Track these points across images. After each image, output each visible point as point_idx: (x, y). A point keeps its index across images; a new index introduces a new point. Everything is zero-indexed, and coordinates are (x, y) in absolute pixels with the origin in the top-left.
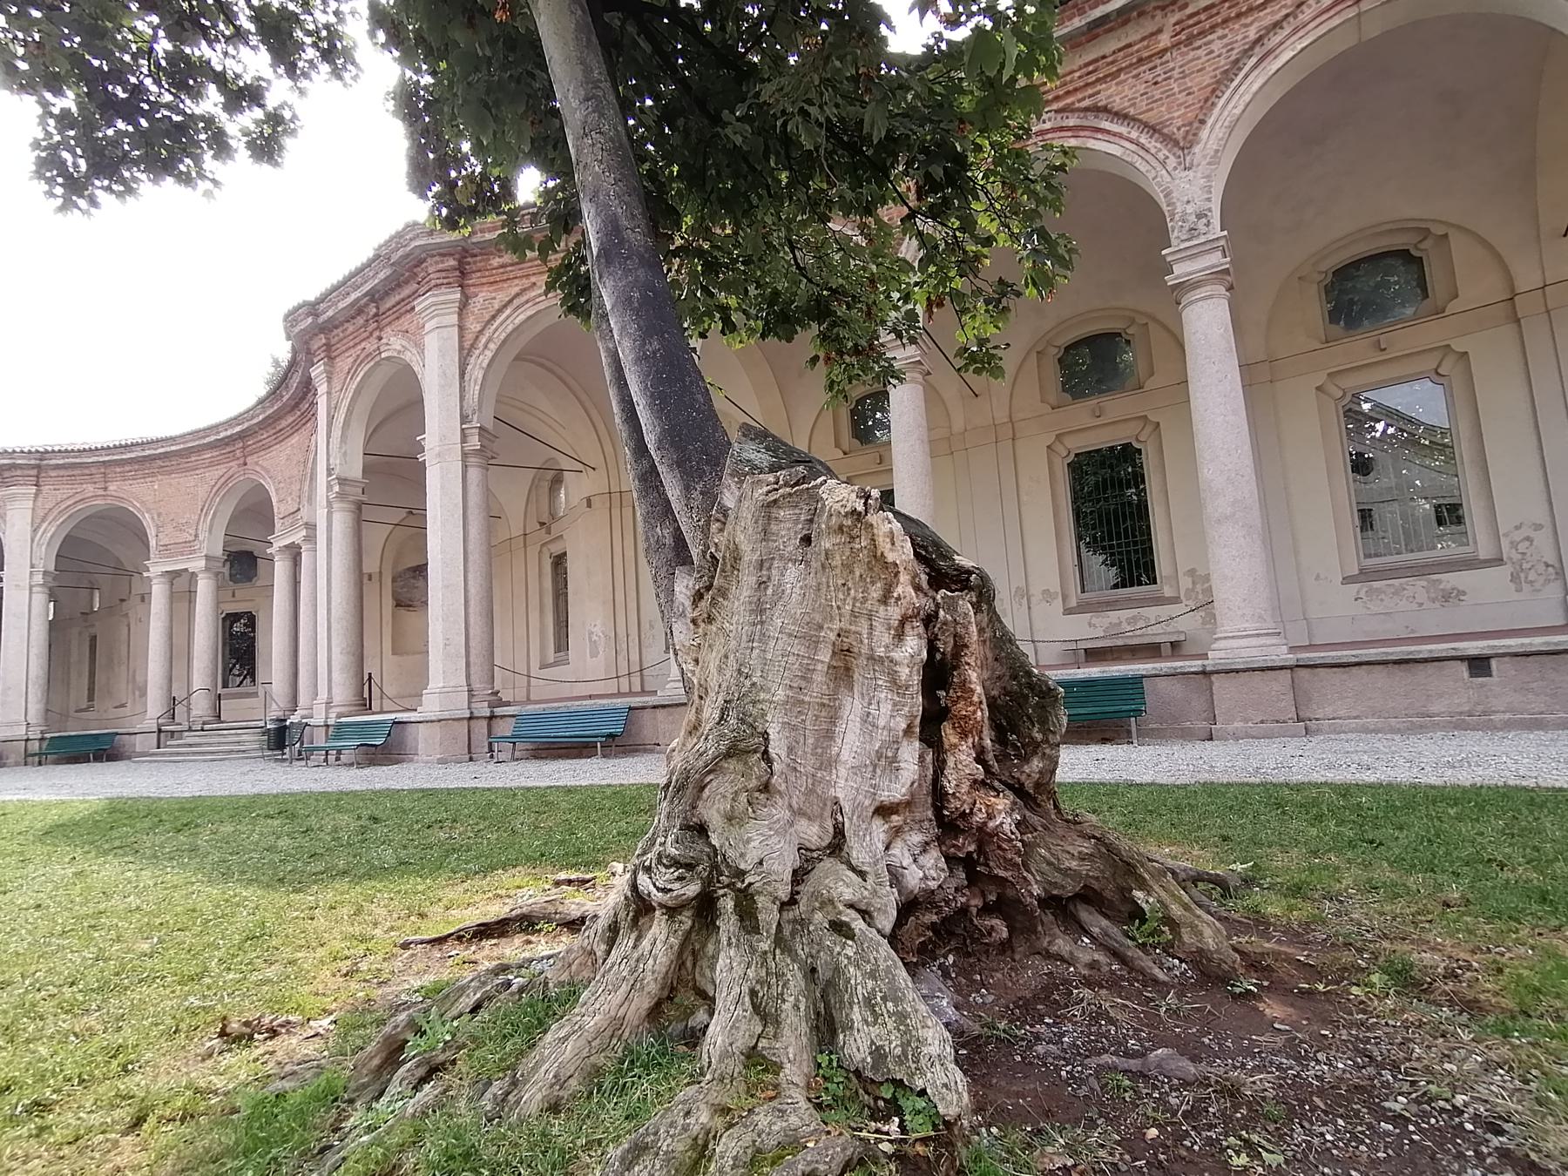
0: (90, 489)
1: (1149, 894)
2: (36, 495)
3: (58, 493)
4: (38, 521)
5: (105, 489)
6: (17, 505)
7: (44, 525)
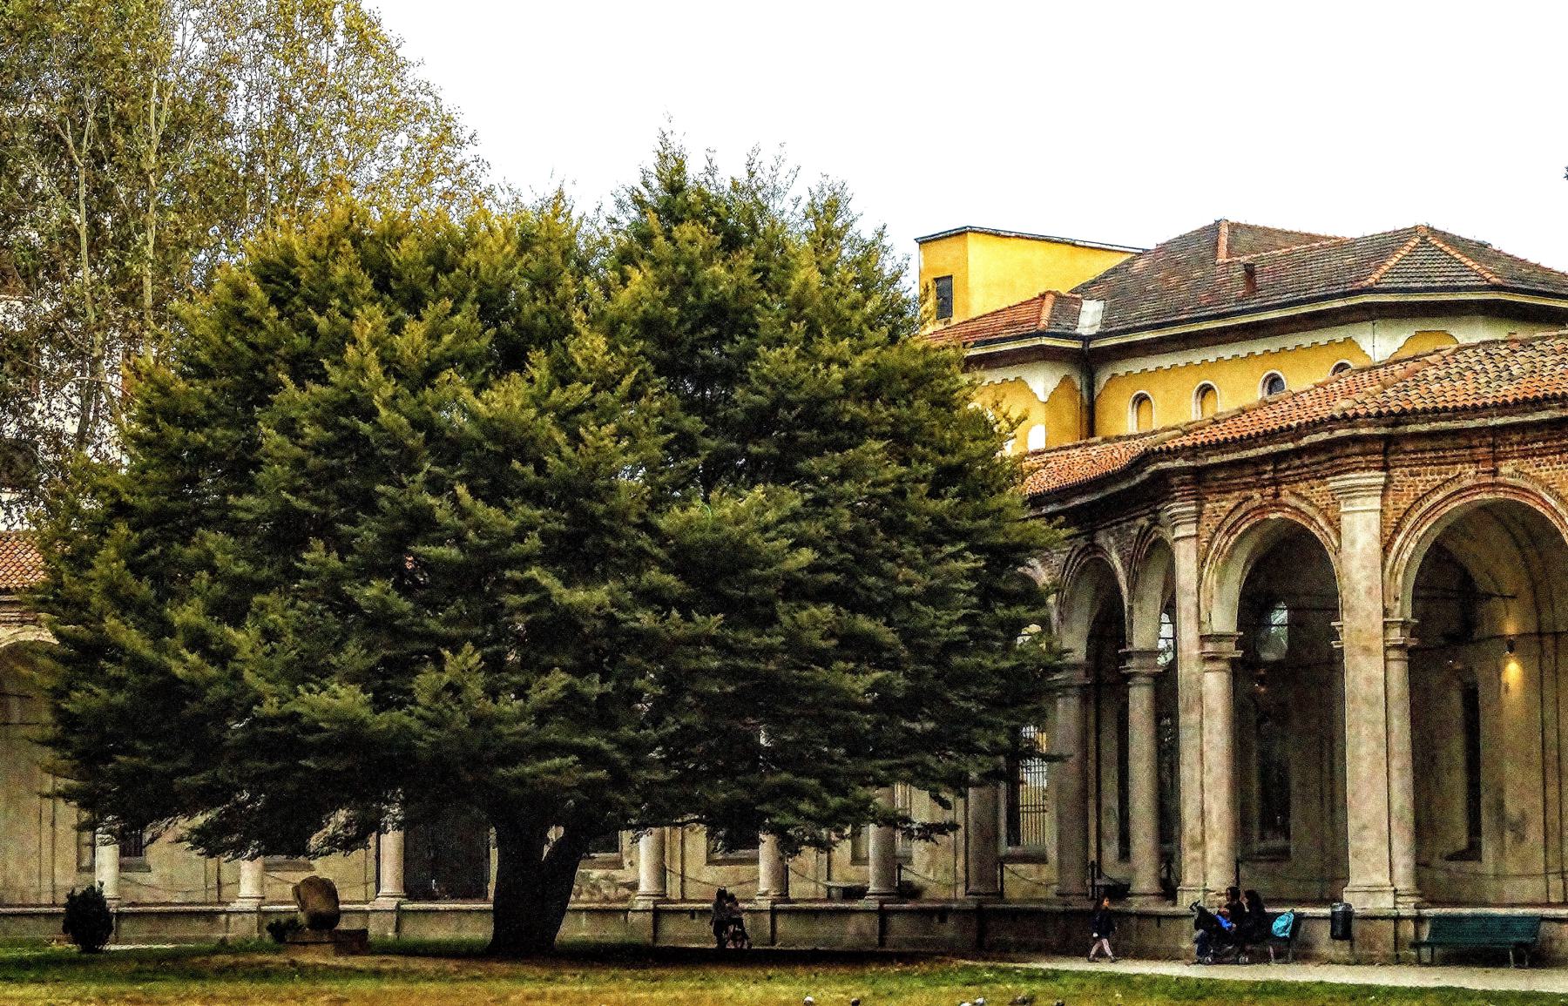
0: (1470, 474)
1: (117, 772)
2: (1386, 487)
3: (1416, 481)
4: (1389, 531)
5: (1495, 473)
6: (1359, 504)
7: (1399, 539)
